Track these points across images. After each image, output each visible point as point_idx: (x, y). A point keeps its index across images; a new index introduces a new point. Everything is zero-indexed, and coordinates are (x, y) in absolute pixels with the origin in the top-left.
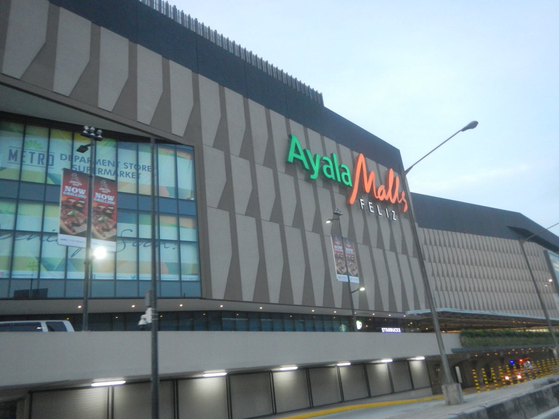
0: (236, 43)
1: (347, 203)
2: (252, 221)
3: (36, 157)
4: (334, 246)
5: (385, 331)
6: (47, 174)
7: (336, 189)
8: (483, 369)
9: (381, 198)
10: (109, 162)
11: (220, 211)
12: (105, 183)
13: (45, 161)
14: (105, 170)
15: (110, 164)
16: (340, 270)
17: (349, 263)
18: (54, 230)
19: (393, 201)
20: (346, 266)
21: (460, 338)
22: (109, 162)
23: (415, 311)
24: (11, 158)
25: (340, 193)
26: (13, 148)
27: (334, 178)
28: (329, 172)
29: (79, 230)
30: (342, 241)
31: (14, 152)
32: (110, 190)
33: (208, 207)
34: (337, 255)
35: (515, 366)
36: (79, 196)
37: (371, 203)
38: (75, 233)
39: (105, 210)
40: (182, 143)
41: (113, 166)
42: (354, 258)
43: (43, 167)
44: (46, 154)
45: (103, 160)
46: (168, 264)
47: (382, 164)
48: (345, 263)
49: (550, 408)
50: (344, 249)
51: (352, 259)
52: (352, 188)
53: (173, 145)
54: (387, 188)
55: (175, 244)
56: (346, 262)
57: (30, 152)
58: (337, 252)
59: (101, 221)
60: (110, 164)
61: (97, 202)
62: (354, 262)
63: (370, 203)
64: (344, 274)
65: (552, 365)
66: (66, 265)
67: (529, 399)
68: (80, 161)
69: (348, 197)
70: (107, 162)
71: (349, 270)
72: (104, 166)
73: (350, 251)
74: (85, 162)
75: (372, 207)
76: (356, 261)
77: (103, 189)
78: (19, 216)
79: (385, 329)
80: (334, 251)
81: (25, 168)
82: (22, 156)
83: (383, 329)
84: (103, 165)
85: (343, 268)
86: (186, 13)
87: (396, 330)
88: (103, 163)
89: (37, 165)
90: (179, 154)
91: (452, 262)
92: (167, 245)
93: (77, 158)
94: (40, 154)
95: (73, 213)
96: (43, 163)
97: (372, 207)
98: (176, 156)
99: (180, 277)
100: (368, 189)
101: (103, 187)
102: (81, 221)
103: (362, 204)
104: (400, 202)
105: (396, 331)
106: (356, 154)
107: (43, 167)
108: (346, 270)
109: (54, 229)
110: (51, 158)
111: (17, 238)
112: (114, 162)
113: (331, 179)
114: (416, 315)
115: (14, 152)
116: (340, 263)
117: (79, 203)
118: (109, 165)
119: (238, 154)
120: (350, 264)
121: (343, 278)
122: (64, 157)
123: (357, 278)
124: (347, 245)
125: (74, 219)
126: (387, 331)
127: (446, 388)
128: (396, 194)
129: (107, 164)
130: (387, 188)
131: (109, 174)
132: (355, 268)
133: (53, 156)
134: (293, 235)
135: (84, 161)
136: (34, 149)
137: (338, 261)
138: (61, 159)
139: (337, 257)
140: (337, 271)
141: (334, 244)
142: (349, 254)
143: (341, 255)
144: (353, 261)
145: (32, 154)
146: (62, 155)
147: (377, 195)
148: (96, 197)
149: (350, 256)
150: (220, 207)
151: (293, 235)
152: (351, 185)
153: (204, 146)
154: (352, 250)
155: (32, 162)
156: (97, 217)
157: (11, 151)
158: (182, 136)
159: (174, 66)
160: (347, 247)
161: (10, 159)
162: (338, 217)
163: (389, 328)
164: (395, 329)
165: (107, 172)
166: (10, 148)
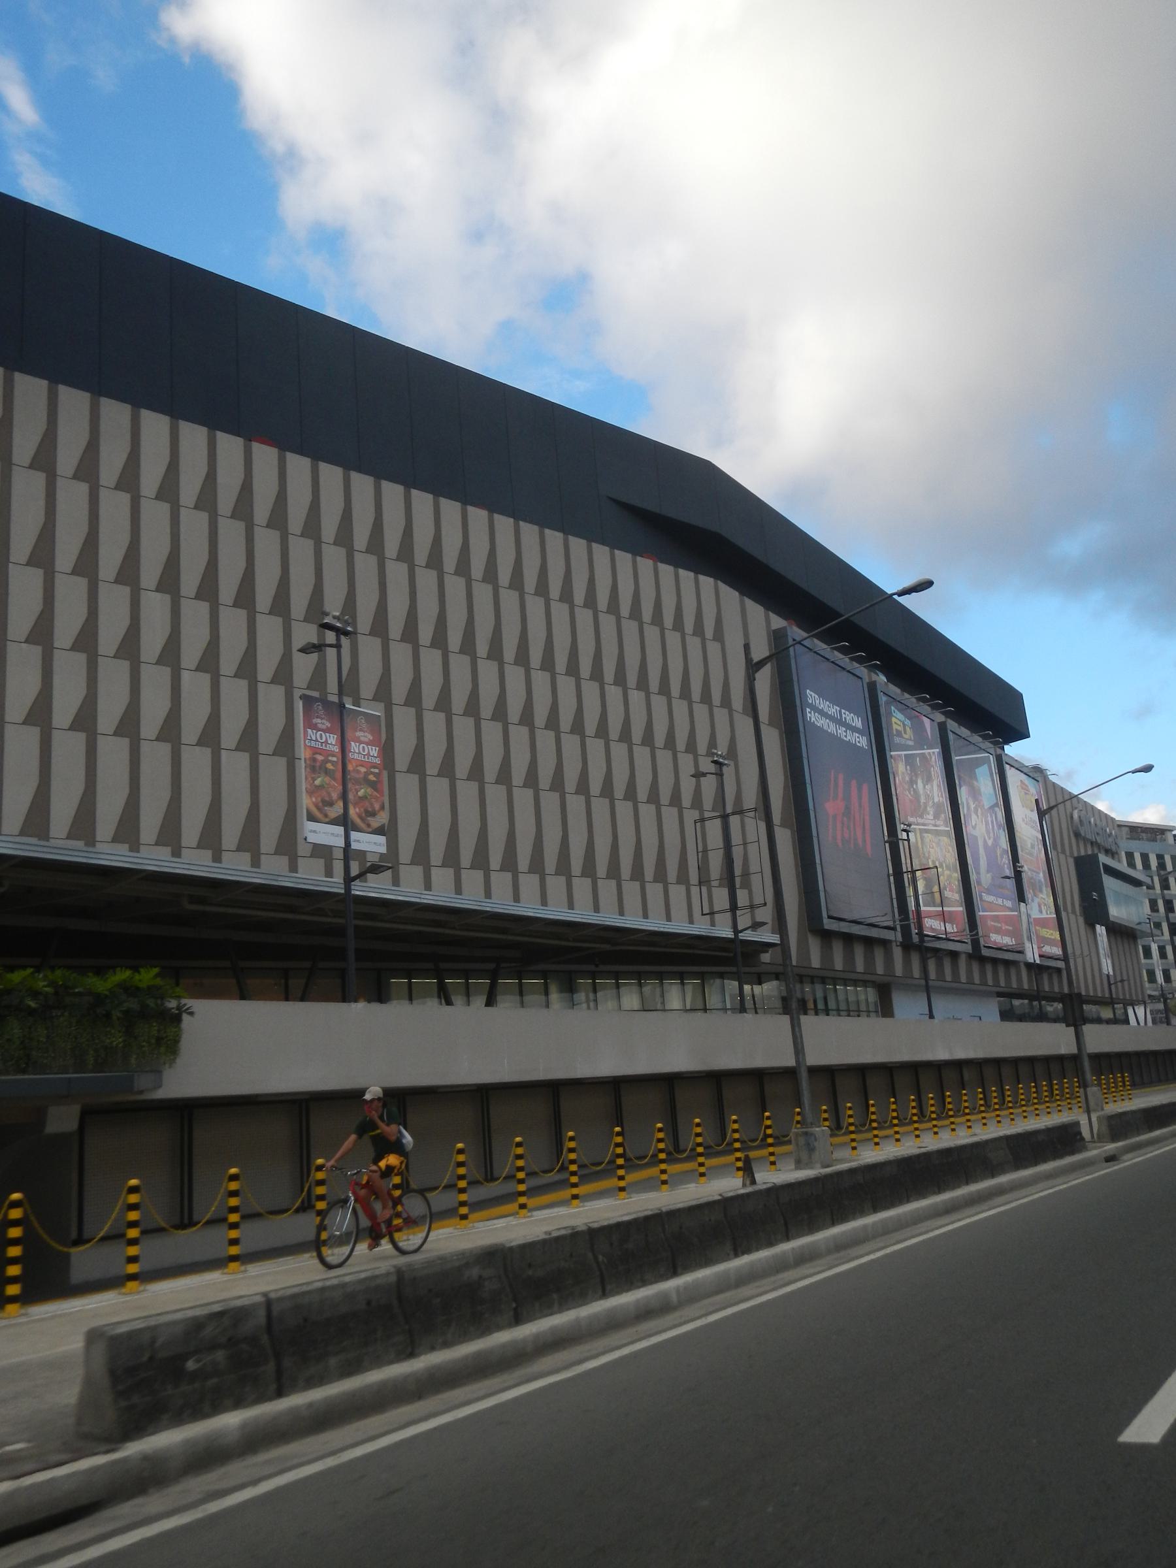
4: (305, 733)
12: (363, 721)
20: (344, 796)
29: (375, 822)
32: (372, 735)
34: (314, 760)
38: (327, 820)
39: (367, 774)
48: (341, 788)
51: (372, 777)
58: (316, 751)
59: (320, 786)
62: (376, 790)
64: (334, 822)
65: (1116, 1087)
71: (353, 812)
77: (319, 721)
95: (323, 781)
101: (361, 730)
108: (341, 811)
116: (321, 787)
123: (382, 839)
124: (359, 734)
125: (367, 804)
132: (377, 806)
137: (314, 779)
141: (309, 725)
144: (374, 785)
154: (374, 751)
156: (356, 789)
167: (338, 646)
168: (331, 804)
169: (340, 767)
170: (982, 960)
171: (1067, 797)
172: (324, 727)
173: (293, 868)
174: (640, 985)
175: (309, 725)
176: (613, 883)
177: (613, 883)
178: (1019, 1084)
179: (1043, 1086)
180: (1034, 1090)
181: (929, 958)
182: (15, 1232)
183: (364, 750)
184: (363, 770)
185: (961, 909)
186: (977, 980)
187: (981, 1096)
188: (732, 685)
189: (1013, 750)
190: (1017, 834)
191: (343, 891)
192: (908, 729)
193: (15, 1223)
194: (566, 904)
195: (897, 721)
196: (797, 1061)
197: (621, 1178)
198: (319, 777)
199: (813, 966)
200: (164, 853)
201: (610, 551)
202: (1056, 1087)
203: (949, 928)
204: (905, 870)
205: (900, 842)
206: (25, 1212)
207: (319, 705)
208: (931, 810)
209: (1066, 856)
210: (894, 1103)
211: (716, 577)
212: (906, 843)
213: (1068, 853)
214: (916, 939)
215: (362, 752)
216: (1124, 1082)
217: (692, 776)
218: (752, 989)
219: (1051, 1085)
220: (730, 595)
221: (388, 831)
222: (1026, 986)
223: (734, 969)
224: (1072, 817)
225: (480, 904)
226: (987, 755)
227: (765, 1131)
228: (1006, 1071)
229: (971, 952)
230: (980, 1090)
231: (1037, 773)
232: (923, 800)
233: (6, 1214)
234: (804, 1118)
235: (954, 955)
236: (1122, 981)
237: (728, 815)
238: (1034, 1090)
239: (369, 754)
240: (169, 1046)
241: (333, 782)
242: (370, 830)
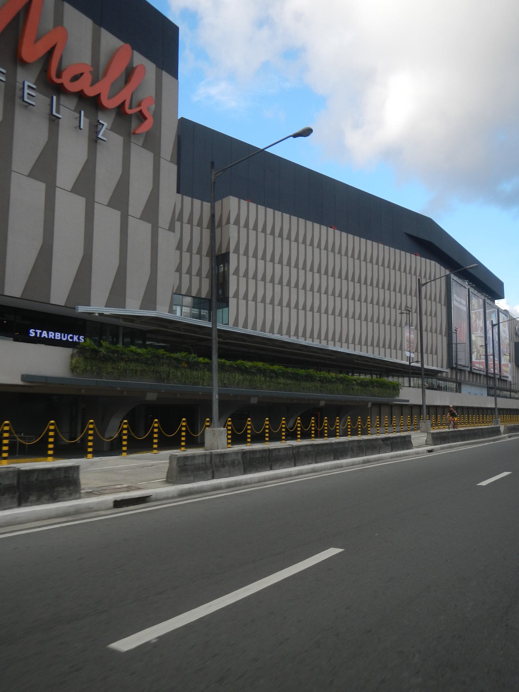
83: (31, 331)
170: (473, 373)
171: (512, 318)
173: (313, 341)
174: (393, 377)
176: (395, 350)
177: (395, 350)
178: (444, 415)
179: (466, 417)
180: (462, 418)
181: (458, 373)
182: (6, 435)
185: (484, 361)
186: (471, 381)
187: (378, 420)
188: (342, 246)
189: (500, 303)
190: (501, 336)
191: (211, 326)
192: (476, 303)
193: (6, 432)
194: (347, 348)
195: (455, 289)
196: (495, 406)
197: (488, 424)
200: (287, 337)
202: (485, 417)
203: (481, 366)
204: (453, 343)
205: (453, 333)
206: (10, 428)
208: (479, 329)
209: (441, 305)
210: (463, 416)
211: (435, 261)
212: (455, 334)
213: (513, 341)
214: (454, 366)
216: (511, 418)
217: (400, 313)
218: (510, 393)
219: (483, 417)
220: (438, 265)
222: (508, 388)
223: (408, 375)
224: (515, 328)
225: (241, 330)
226: (495, 309)
227: (282, 426)
228: (440, 411)
229: (469, 370)
230: (478, 416)
231: (506, 312)
232: (478, 326)
233: (3, 429)
234: (423, 418)
235: (480, 375)
236: (515, 384)
237: (457, 344)
238: (478, 418)
240: (398, 394)
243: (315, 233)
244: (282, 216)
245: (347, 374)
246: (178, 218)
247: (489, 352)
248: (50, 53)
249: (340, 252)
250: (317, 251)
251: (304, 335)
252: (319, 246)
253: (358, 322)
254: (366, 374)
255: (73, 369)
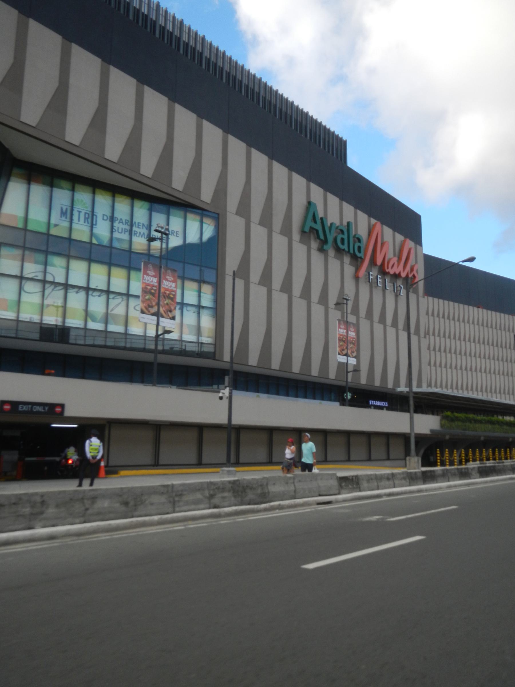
0: (295, 103)
1: (355, 276)
2: (264, 290)
3: (82, 216)
5: (373, 404)
6: (92, 234)
7: (347, 260)
8: (463, 450)
9: (392, 272)
10: (143, 225)
11: (300, 299)
12: (151, 266)
13: (90, 220)
14: (140, 233)
15: (144, 227)
16: (341, 351)
17: (350, 345)
18: (97, 286)
19: (403, 275)
20: (158, 304)
21: (441, 420)
22: (143, 225)
23: (405, 388)
24: (63, 216)
25: (350, 264)
26: (83, 224)
27: (347, 249)
28: (343, 243)
30: (347, 325)
31: (64, 210)
33: (226, 275)
35: (456, 451)
36: (152, 284)
37: (380, 277)
39: (169, 294)
40: (209, 210)
41: (147, 229)
42: (355, 341)
43: (88, 226)
44: (90, 213)
45: (138, 223)
46: (189, 326)
47: (398, 232)
49: (470, 478)
50: (347, 332)
52: (363, 260)
53: (200, 211)
54: (400, 259)
55: (196, 308)
56: (347, 345)
57: (78, 211)
60: (144, 227)
61: (164, 288)
63: (379, 276)
64: (153, 314)
66: (106, 319)
67: (456, 471)
68: (119, 222)
69: (357, 270)
70: (141, 225)
71: (162, 310)
72: (139, 229)
73: (352, 334)
74: (123, 224)
75: (380, 281)
76: (356, 344)
78: (70, 272)
79: (372, 401)
80: (338, 333)
81: (74, 226)
82: (72, 215)
83: (370, 401)
84: (138, 227)
85: (343, 350)
86: (215, 44)
87: (383, 404)
88: (138, 225)
89: (84, 224)
90: (205, 220)
91: (457, 338)
92: (189, 308)
93: (116, 219)
94: (85, 213)
96: (88, 223)
97: (380, 281)
98: (202, 222)
99: (198, 339)
100: (379, 262)
102: (154, 304)
103: (371, 277)
104: (410, 276)
105: (383, 405)
106: (373, 221)
107: (88, 226)
109: (96, 285)
110: (95, 217)
111: (68, 291)
112: (147, 225)
113: (344, 250)
114: (406, 392)
115: (64, 210)
117: (152, 289)
118: (143, 228)
119: (258, 222)
120: (351, 346)
121: (342, 359)
122: (105, 218)
123: (355, 360)
126: (374, 403)
127: (410, 459)
128: (408, 268)
129: (141, 227)
130: (400, 259)
131: (143, 237)
133: (96, 216)
134: (300, 306)
135: (122, 223)
136: (80, 208)
137: (340, 343)
138: (103, 219)
139: (340, 340)
140: (338, 352)
141: (339, 328)
142: (351, 338)
143: (344, 338)
144: (354, 344)
145: (79, 212)
146: (104, 215)
147: (388, 268)
148: (164, 284)
149: (351, 339)
150: (260, 283)
151: (300, 306)
152: (363, 257)
153: (228, 214)
155: (79, 220)
157: (62, 209)
158: (209, 203)
159: (207, 125)
160: (351, 331)
161: (61, 217)
162: (347, 302)
163: (376, 402)
164: (383, 402)
165: (141, 235)
166: (62, 206)
167: (347, 304)
168: (152, 307)
169: (157, 292)
172: (152, 275)
175: (339, 328)
183: (150, 279)
184: (351, 339)
198: (147, 295)
199: (294, 371)
201: (247, 149)
207: (150, 265)
215: (149, 280)
221: (357, 357)
239: (171, 286)
241: (154, 298)
242: (149, 313)
243: (451, 309)
244: (444, 302)
245: (493, 416)
246: (352, 310)
247: (80, 325)
248: (314, 216)
249: (483, 325)
250: (472, 326)
251: (441, 386)
252: (473, 323)
253: (449, 370)
254: (510, 416)
255: (442, 426)
